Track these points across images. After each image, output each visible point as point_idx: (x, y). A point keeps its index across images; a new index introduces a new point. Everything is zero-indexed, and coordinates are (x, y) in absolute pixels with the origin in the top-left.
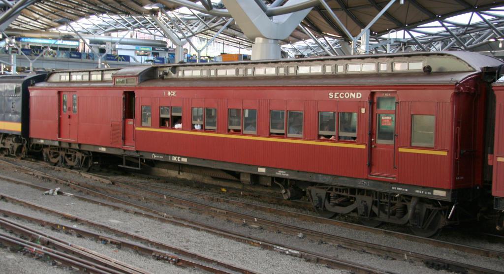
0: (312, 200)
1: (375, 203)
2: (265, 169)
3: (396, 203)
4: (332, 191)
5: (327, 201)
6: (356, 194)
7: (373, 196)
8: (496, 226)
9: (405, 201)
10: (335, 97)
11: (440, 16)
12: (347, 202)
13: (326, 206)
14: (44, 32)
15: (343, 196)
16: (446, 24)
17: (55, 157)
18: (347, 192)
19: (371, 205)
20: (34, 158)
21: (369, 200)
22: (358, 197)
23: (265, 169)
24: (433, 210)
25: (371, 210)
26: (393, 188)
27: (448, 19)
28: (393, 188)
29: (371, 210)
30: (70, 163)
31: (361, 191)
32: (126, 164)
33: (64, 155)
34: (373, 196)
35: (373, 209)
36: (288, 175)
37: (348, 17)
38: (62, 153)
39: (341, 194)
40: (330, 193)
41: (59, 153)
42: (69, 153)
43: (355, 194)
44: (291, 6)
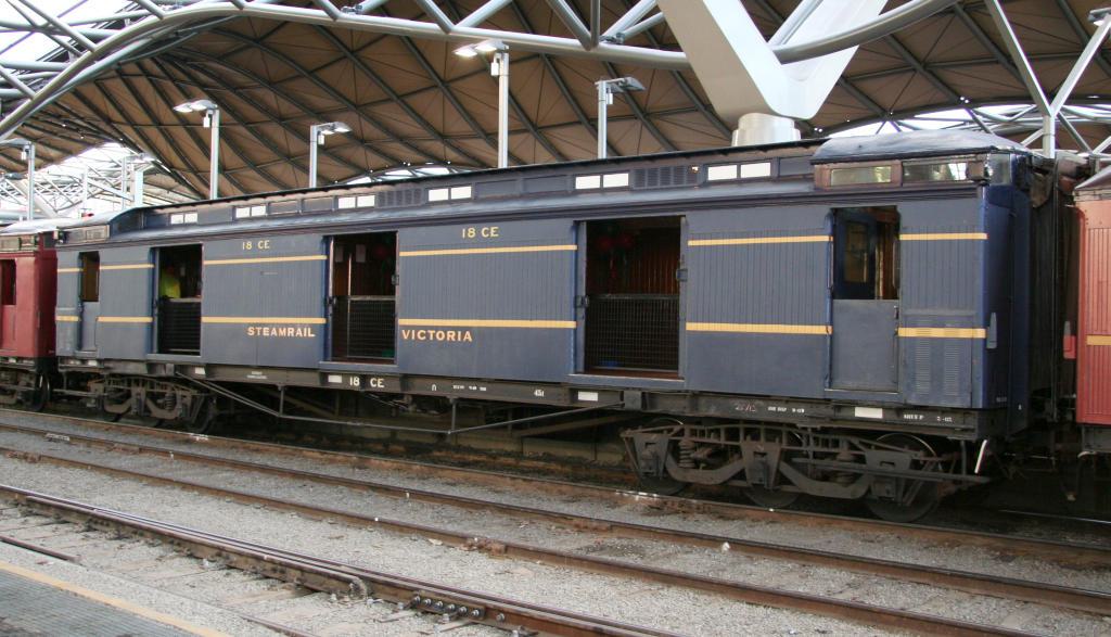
0: (636, 457)
1: (787, 456)
2: (881, 410)
3: (837, 454)
4: (683, 435)
5: (670, 458)
6: (742, 437)
7: (781, 441)
8: (1065, 498)
9: (861, 447)
10: (492, 235)
11: (967, 101)
12: (720, 456)
13: (670, 470)
14: (181, 27)
15: (709, 445)
16: (980, 118)
17: (120, 402)
18: (719, 436)
19: (776, 461)
20: (632, 490)
21: (773, 450)
22: (747, 446)
23: (881, 410)
24: (925, 462)
25: (778, 471)
26: (536, 393)
27: (981, 109)
28: (455, 387)
29: (778, 471)
30: (157, 413)
31: (753, 429)
32: (285, 412)
33: (143, 397)
34: (781, 441)
35: (781, 469)
36: (455, 387)
37: (537, 143)
38: (139, 391)
39: (705, 440)
40: (679, 441)
41: (129, 391)
42: (157, 390)
43: (738, 440)
44: (819, 42)
